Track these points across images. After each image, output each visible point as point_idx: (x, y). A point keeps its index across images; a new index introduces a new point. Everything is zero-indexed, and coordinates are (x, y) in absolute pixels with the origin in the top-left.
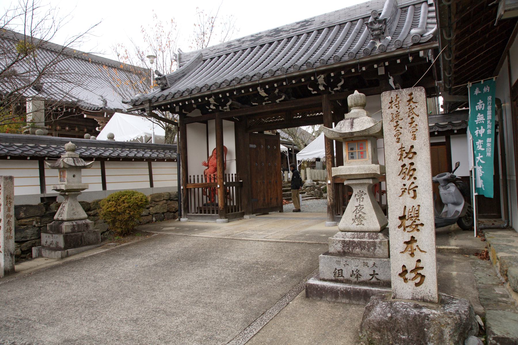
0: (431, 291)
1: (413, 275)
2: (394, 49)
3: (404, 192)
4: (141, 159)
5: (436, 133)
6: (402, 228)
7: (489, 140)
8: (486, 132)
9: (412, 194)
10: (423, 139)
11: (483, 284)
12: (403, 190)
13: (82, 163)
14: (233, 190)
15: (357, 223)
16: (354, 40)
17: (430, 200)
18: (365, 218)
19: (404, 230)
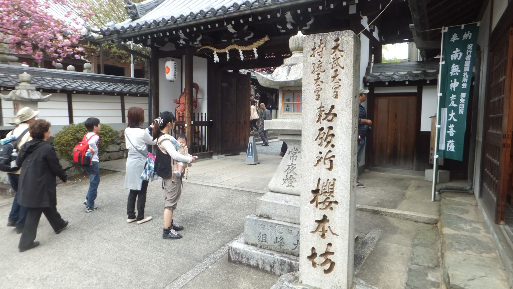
0: (341, 281)
1: (323, 260)
3: (319, 161)
4: (112, 93)
5: (407, 83)
6: (314, 204)
7: (463, 95)
8: (460, 85)
9: (328, 165)
11: (418, 265)
12: (319, 159)
13: (37, 95)
14: (204, 130)
15: (287, 185)
17: (347, 175)
18: (296, 179)
19: (317, 206)
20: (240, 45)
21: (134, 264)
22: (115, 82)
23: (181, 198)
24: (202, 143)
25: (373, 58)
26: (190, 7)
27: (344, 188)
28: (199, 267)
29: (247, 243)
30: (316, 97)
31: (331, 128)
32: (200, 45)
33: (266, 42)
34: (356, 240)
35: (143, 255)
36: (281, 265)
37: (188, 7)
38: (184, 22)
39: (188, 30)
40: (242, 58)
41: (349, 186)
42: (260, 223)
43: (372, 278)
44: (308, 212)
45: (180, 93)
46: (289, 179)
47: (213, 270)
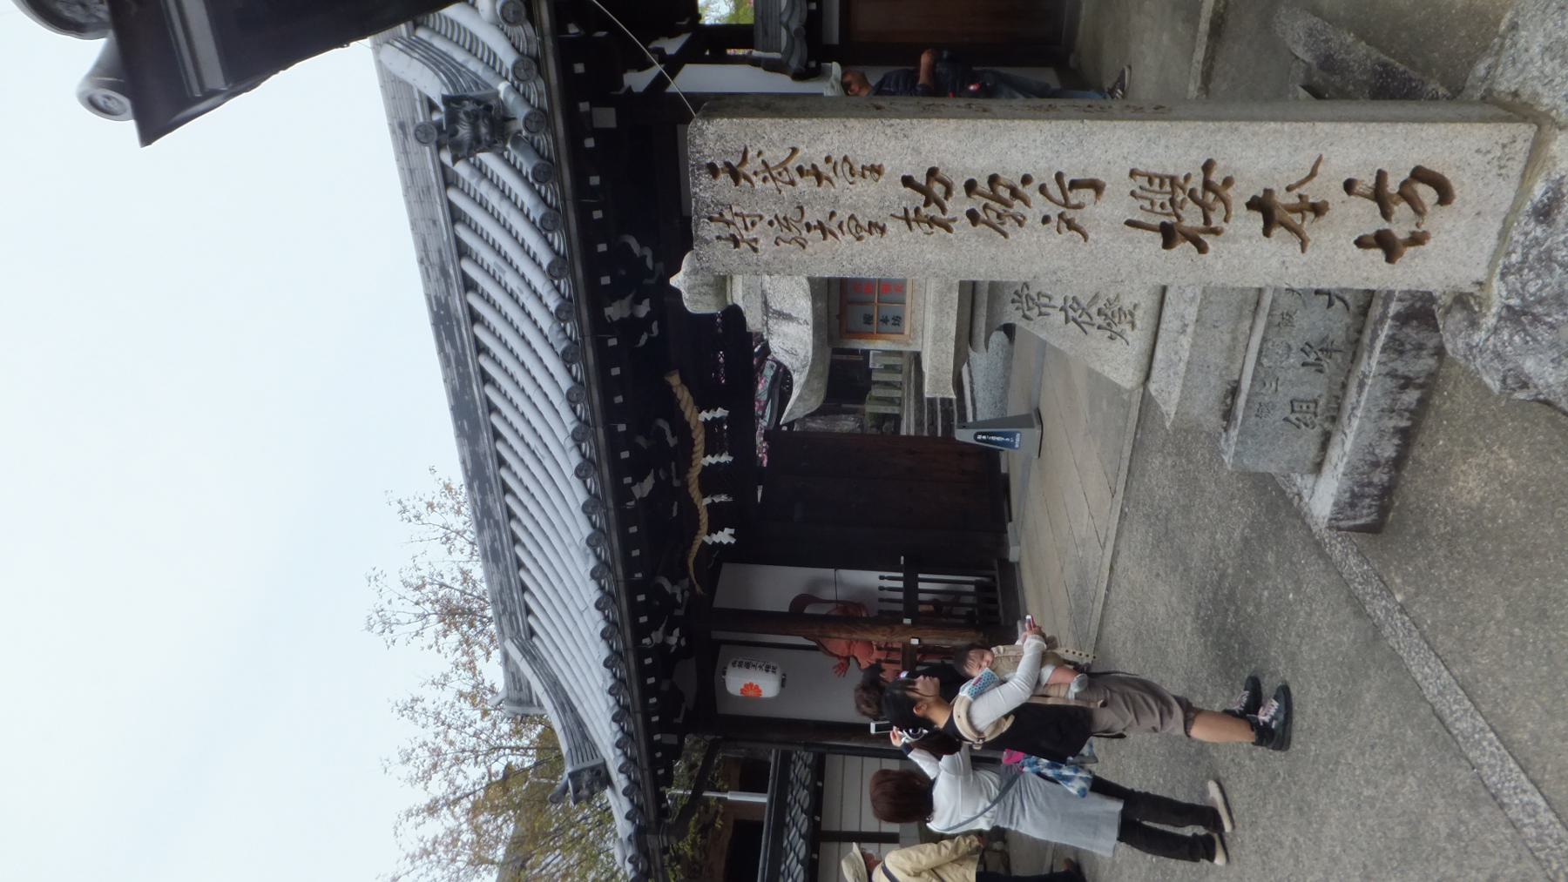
0: (1484, 146)
1: (1402, 210)
2: (541, 85)
3: (1071, 225)
6: (1208, 239)
9: (1088, 194)
10: (882, 138)
12: (1063, 225)
14: (930, 585)
15: (1128, 327)
16: (505, 194)
17: (1119, 132)
18: (1112, 296)
19: (1216, 232)
20: (688, 462)
21: (1380, 864)
22: (778, 855)
23: (1146, 676)
24: (968, 593)
25: (741, 52)
26: (582, 608)
27: (1163, 142)
28: (1398, 634)
29: (1318, 468)
30: (876, 234)
31: (970, 187)
32: (686, 582)
33: (684, 381)
34: (1317, 93)
35: (1346, 825)
36: (1401, 353)
37: (581, 613)
38: (621, 631)
39: (643, 619)
40: (725, 458)
41: (1155, 124)
42: (1253, 419)
43: (1463, 33)
44: (1236, 262)
45: (819, 656)
46: (1111, 319)
47: (1412, 590)
